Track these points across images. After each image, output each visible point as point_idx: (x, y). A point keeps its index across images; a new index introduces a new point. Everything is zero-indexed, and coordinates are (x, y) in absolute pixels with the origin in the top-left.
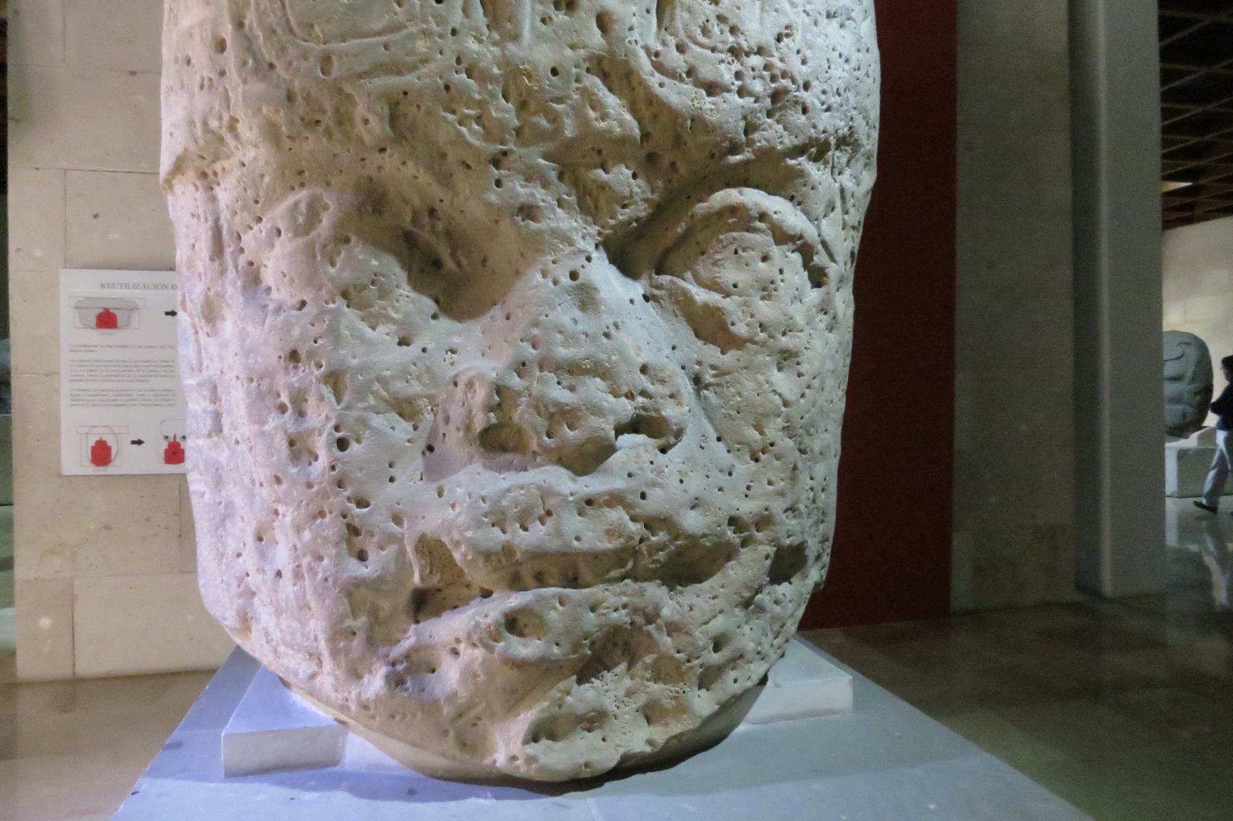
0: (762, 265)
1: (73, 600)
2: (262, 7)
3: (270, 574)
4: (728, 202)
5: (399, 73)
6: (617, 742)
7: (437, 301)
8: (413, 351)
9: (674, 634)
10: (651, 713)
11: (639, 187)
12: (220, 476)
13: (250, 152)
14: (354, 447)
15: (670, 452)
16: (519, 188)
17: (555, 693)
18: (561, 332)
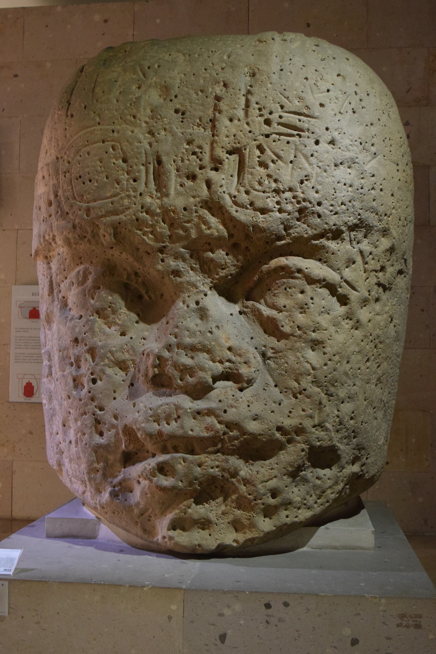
0: (300, 296)
1: (13, 473)
2: (64, 188)
3: (68, 442)
4: (279, 264)
5: (117, 214)
6: (217, 537)
7: (138, 315)
8: (127, 338)
9: (247, 485)
10: (237, 525)
11: (229, 260)
12: (51, 396)
13: (61, 250)
14: (99, 382)
15: (245, 391)
16: (171, 263)
17: (182, 506)
18: (188, 331)
